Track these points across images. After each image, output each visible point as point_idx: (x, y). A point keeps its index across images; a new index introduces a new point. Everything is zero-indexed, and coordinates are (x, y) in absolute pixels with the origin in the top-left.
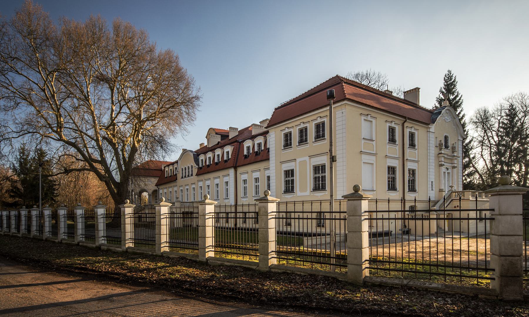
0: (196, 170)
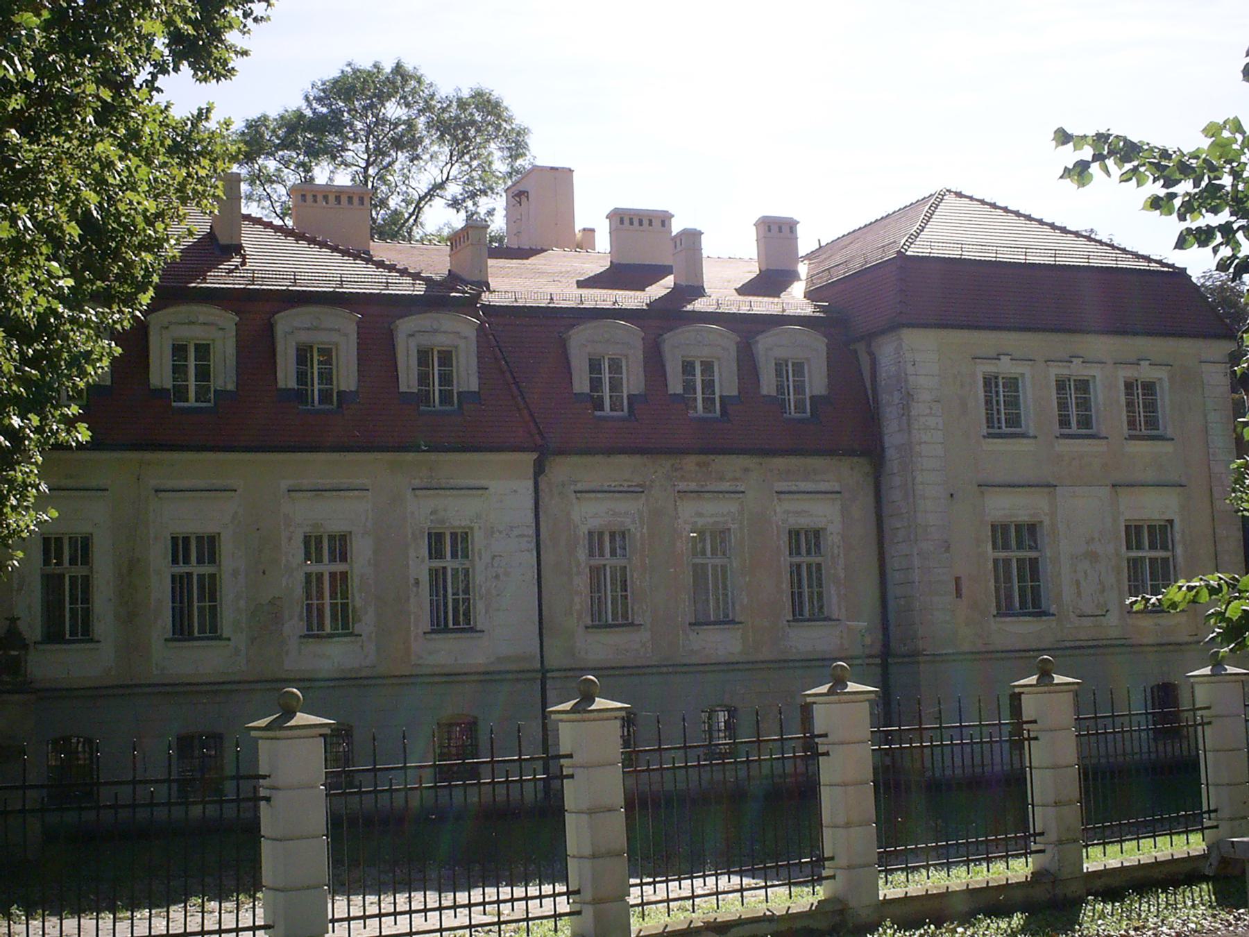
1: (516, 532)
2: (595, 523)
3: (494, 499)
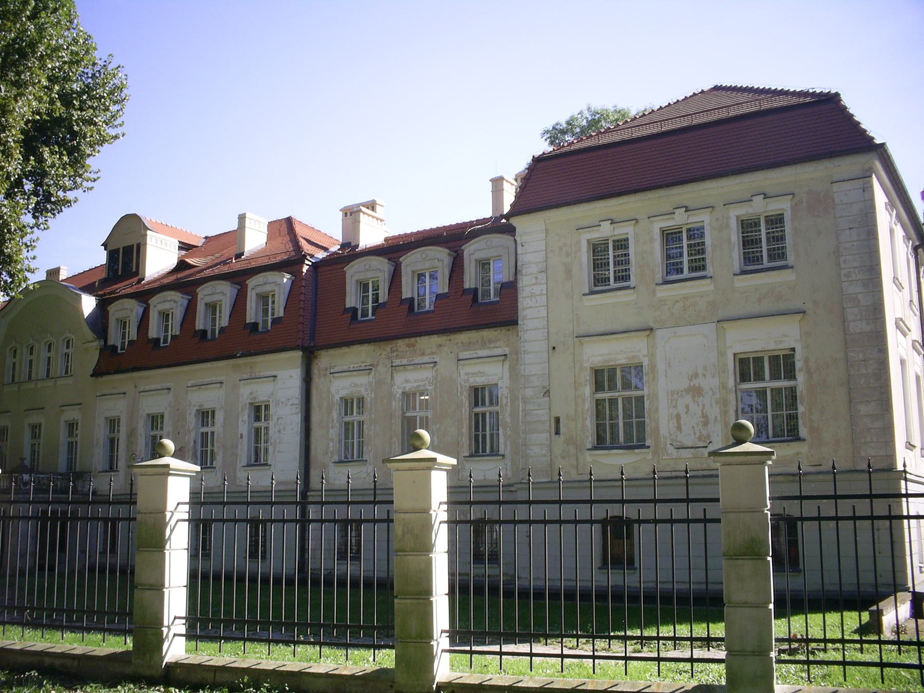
0: (96, 355)
1: (291, 402)
2: (343, 393)
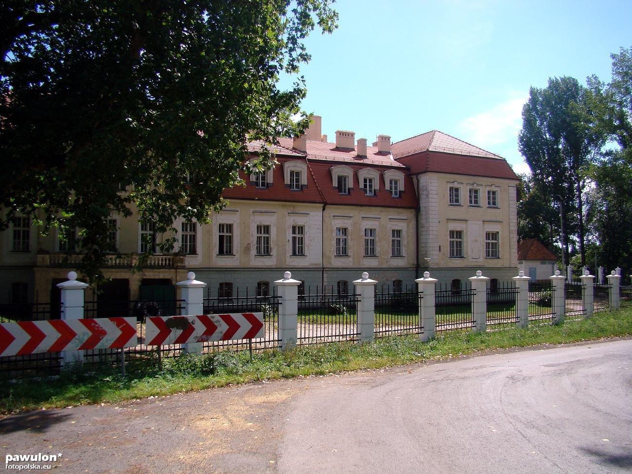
3: (312, 219)
